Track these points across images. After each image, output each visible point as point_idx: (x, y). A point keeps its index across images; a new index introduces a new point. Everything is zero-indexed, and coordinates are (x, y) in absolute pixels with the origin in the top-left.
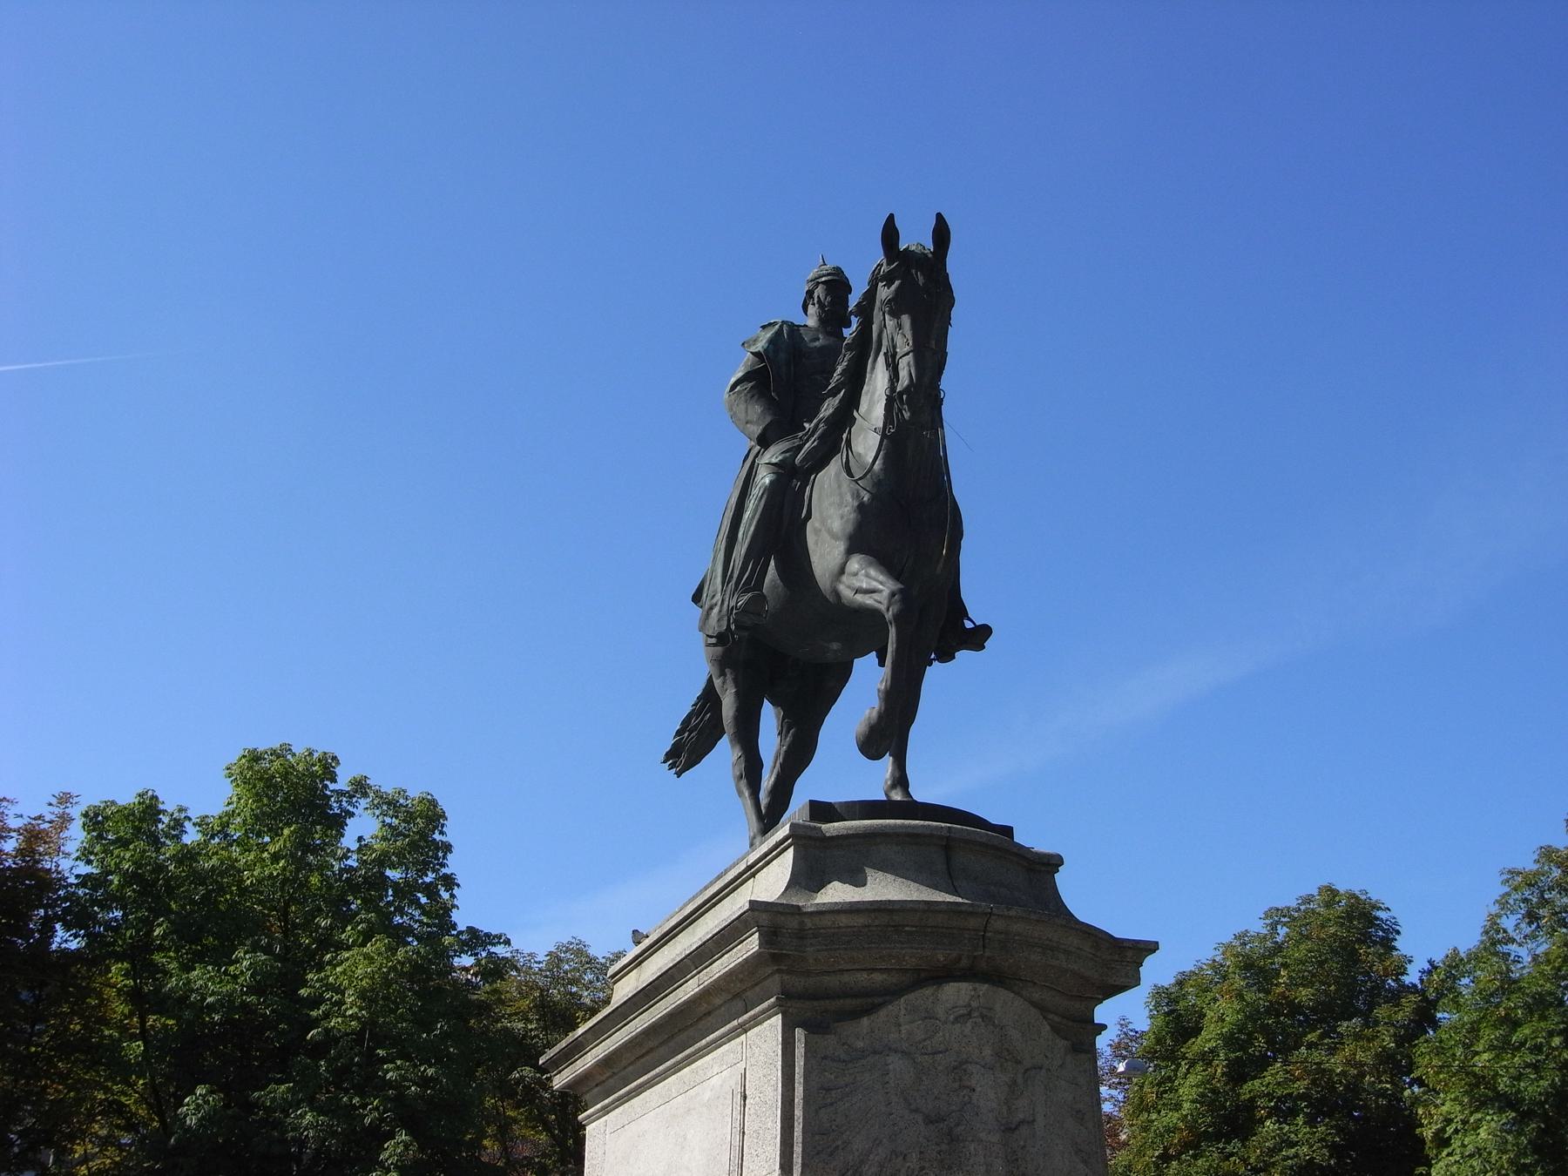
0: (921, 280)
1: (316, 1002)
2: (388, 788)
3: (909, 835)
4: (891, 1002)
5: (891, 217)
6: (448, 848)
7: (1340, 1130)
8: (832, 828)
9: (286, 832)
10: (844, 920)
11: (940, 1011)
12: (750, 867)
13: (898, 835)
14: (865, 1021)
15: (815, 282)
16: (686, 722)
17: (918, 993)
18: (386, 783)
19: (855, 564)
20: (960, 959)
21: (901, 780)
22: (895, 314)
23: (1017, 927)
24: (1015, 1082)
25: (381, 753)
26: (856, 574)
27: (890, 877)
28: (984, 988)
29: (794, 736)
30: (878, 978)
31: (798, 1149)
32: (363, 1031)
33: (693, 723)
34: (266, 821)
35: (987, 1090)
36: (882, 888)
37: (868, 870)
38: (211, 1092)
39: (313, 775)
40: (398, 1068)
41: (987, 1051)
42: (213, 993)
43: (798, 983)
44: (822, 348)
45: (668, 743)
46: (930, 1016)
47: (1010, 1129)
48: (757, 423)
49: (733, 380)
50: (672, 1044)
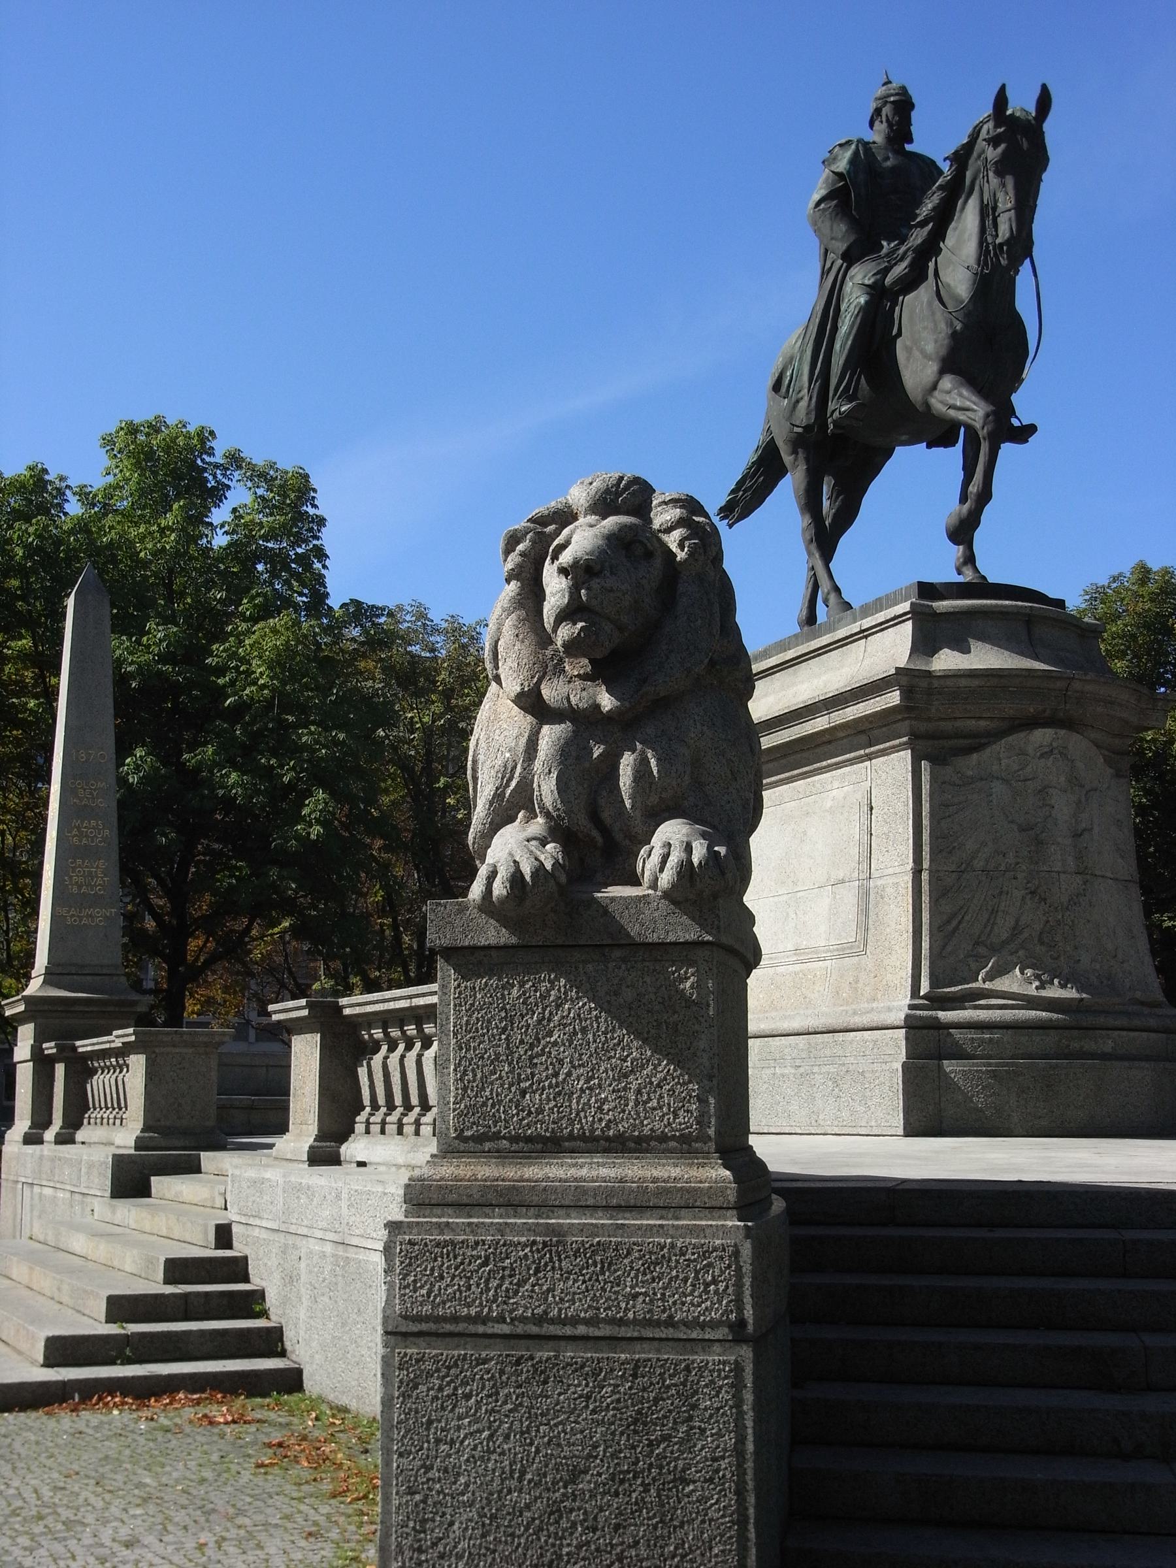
0: (1025, 145)
1: (221, 671)
2: (259, 461)
3: (1001, 613)
4: (995, 743)
6: (321, 521)
7: (1148, 792)
9: (175, 506)
11: (1030, 751)
14: (975, 756)
15: (884, 100)
16: (740, 484)
17: (1015, 736)
18: (257, 456)
19: (947, 382)
20: (1044, 711)
21: (970, 559)
22: (1000, 173)
23: (1089, 688)
24: (1080, 801)
25: (250, 427)
26: (949, 392)
27: (988, 646)
28: (1062, 732)
30: (983, 723)
31: (926, 849)
32: (273, 698)
33: (748, 484)
34: (153, 499)
35: (1062, 806)
36: (984, 657)
37: (970, 640)
38: (147, 754)
39: (192, 450)
40: (311, 733)
41: (1062, 779)
42: (133, 663)
43: (923, 727)
44: (893, 169)
46: (1022, 753)
47: (1077, 835)
50: (783, 761)
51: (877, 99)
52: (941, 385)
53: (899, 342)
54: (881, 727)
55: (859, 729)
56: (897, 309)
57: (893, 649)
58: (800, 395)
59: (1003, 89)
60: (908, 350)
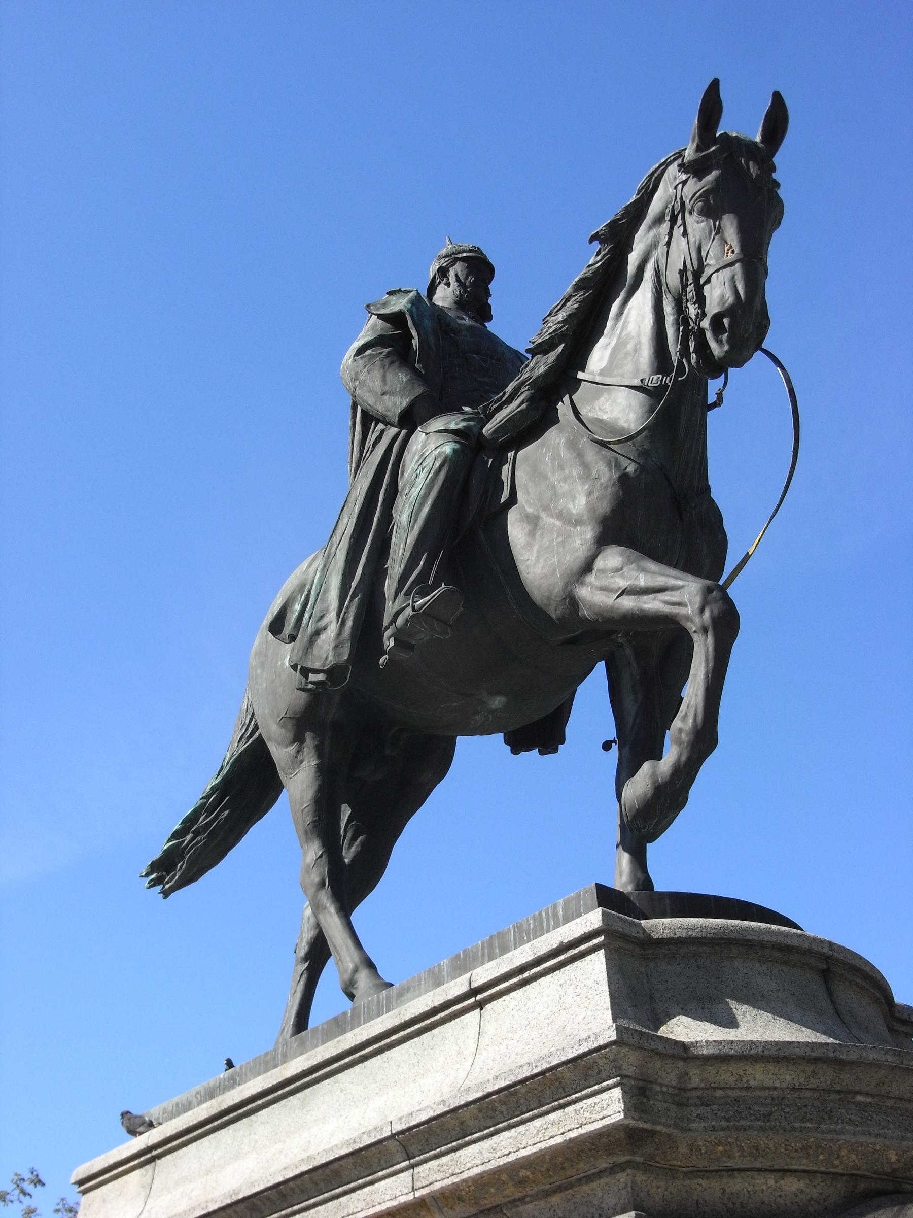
5: (715, 84)
8: (663, 926)
10: (759, 1075)
12: (474, 992)
13: (762, 945)
16: (189, 822)
29: (363, 844)
36: (757, 1027)
45: (158, 847)
48: (401, 393)
49: (357, 344)
51: (440, 258)
52: (599, 563)
53: (512, 515)
54: (547, 1194)
55: (487, 1203)
56: (506, 470)
57: (576, 1009)
58: (323, 623)
59: (715, 86)
60: (533, 521)
